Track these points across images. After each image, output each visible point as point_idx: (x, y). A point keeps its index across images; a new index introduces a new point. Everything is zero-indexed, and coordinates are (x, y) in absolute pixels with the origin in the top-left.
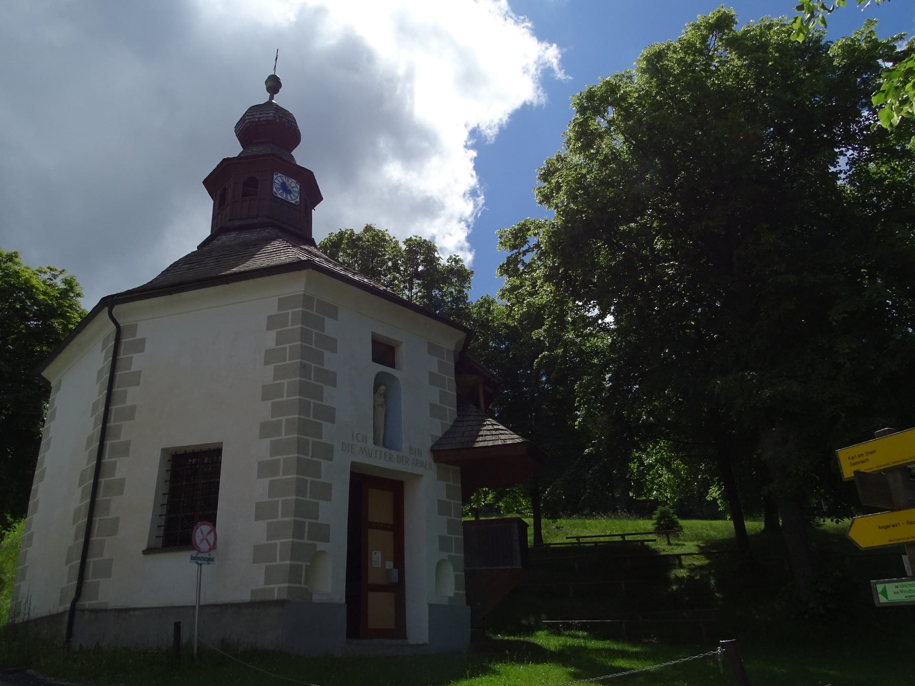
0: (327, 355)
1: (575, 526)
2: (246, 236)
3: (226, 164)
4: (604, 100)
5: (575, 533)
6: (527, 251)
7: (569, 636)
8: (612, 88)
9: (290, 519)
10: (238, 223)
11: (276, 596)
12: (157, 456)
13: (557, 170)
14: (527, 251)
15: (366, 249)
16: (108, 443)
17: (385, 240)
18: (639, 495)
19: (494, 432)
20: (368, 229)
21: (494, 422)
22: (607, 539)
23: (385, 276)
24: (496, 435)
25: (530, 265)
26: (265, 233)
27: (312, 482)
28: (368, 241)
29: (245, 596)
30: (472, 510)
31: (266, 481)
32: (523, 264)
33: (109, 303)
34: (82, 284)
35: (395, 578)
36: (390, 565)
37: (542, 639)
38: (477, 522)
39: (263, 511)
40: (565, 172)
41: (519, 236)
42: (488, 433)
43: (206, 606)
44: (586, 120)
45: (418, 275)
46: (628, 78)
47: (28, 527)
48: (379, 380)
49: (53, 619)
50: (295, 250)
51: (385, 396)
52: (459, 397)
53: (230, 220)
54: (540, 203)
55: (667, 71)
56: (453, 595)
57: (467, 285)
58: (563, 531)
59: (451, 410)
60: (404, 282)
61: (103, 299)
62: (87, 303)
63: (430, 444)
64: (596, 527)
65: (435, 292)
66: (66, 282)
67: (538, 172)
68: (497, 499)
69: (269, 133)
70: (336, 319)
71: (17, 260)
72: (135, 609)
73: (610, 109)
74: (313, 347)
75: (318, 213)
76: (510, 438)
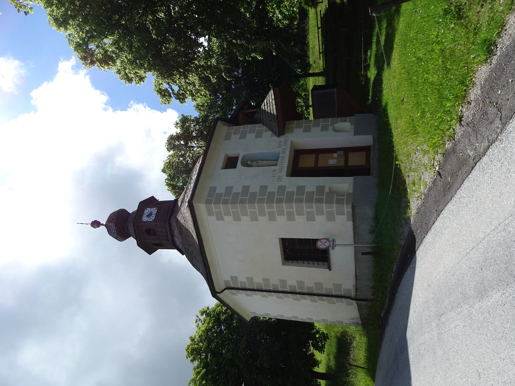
0: (234, 191)
1: (313, 53)
2: (176, 232)
4: (85, 51)
5: (317, 54)
6: (171, 89)
7: (370, 60)
8: (78, 47)
9: (314, 205)
10: (170, 237)
12: (285, 267)
13: (126, 74)
14: (171, 89)
15: (177, 172)
16: (280, 289)
17: (170, 162)
18: (296, 18)
19: (268, 105)
20: (164, 171)
21: (263, 104)
22: (320, 35)
23: (188, 160)
24: (269, 103)
25: (179, 87)
26: (174, 224)
27: (296, 195)
28: (171, 171)
29: (350, 224)
30: (306, 110)
31: (297, 217)
32: (179, 90)
33: (214, 294)
34: (203, 306)
35: (341, 153)
36: (335, 155)
37: (372, 73)
38: (313, 106)
39: (311, 218)
40: (127, 71)
41: (164, 94)
42: (269, 108)
43: (354, 241)
44: (98, 60)
45: (186, 144)
46: (70, 36)
47: (318, 321)
48: (245, 164)
49: (360, 308)
50: (182, 209)
51: (252, 161)
52: (251, 123)
54: (143, 81)
55: (65, 14)
56: (350, 124)
57: (189, 117)
58: (316, 58)
59: (258, 127)
60: (190, 150)
62: (212, 302)
63: (276, 137)
64: (314, 41)
65: (194, 134)
66: (202, 314)
67: (128, 84)
68: (300, 96)
69: (121, 225)
70: (216, 187)
71: (193, 337)
72: (356, 273)
73: (90, 47)
75: (161, 198)
76: (271, 96)
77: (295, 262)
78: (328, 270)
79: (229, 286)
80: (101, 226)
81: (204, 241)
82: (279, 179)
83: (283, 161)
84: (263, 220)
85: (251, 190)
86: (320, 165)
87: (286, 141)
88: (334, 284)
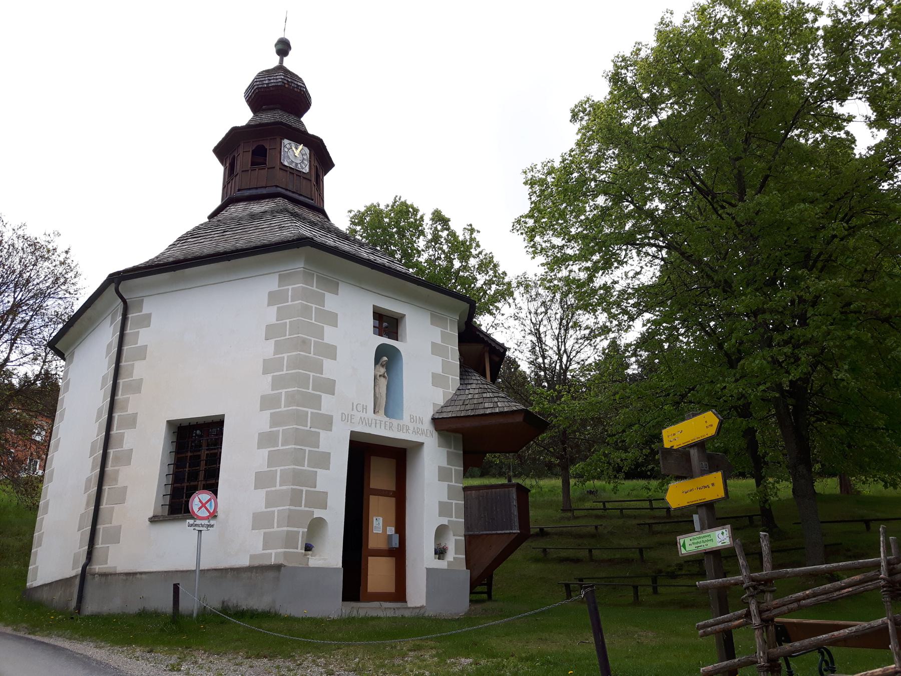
10: (247, 193)
11: (273, 561)
16: (116, 415)
29: (244, 561)
35: (395, 543)
36: (391, 530)
48: (381, 352)
49: (65, 583)
52: (462, 366)
59: (454, 378)
61: (111, 275)
69: (279, 98)
72: (141, 573)
74: (313, 321)
78: (151, 515)
79: (130, 310)
80: (278, 58)
81: (227, 262)
82: (346, 418)
83: (378, 426)
84: (265, 384)
85: (327, 363)
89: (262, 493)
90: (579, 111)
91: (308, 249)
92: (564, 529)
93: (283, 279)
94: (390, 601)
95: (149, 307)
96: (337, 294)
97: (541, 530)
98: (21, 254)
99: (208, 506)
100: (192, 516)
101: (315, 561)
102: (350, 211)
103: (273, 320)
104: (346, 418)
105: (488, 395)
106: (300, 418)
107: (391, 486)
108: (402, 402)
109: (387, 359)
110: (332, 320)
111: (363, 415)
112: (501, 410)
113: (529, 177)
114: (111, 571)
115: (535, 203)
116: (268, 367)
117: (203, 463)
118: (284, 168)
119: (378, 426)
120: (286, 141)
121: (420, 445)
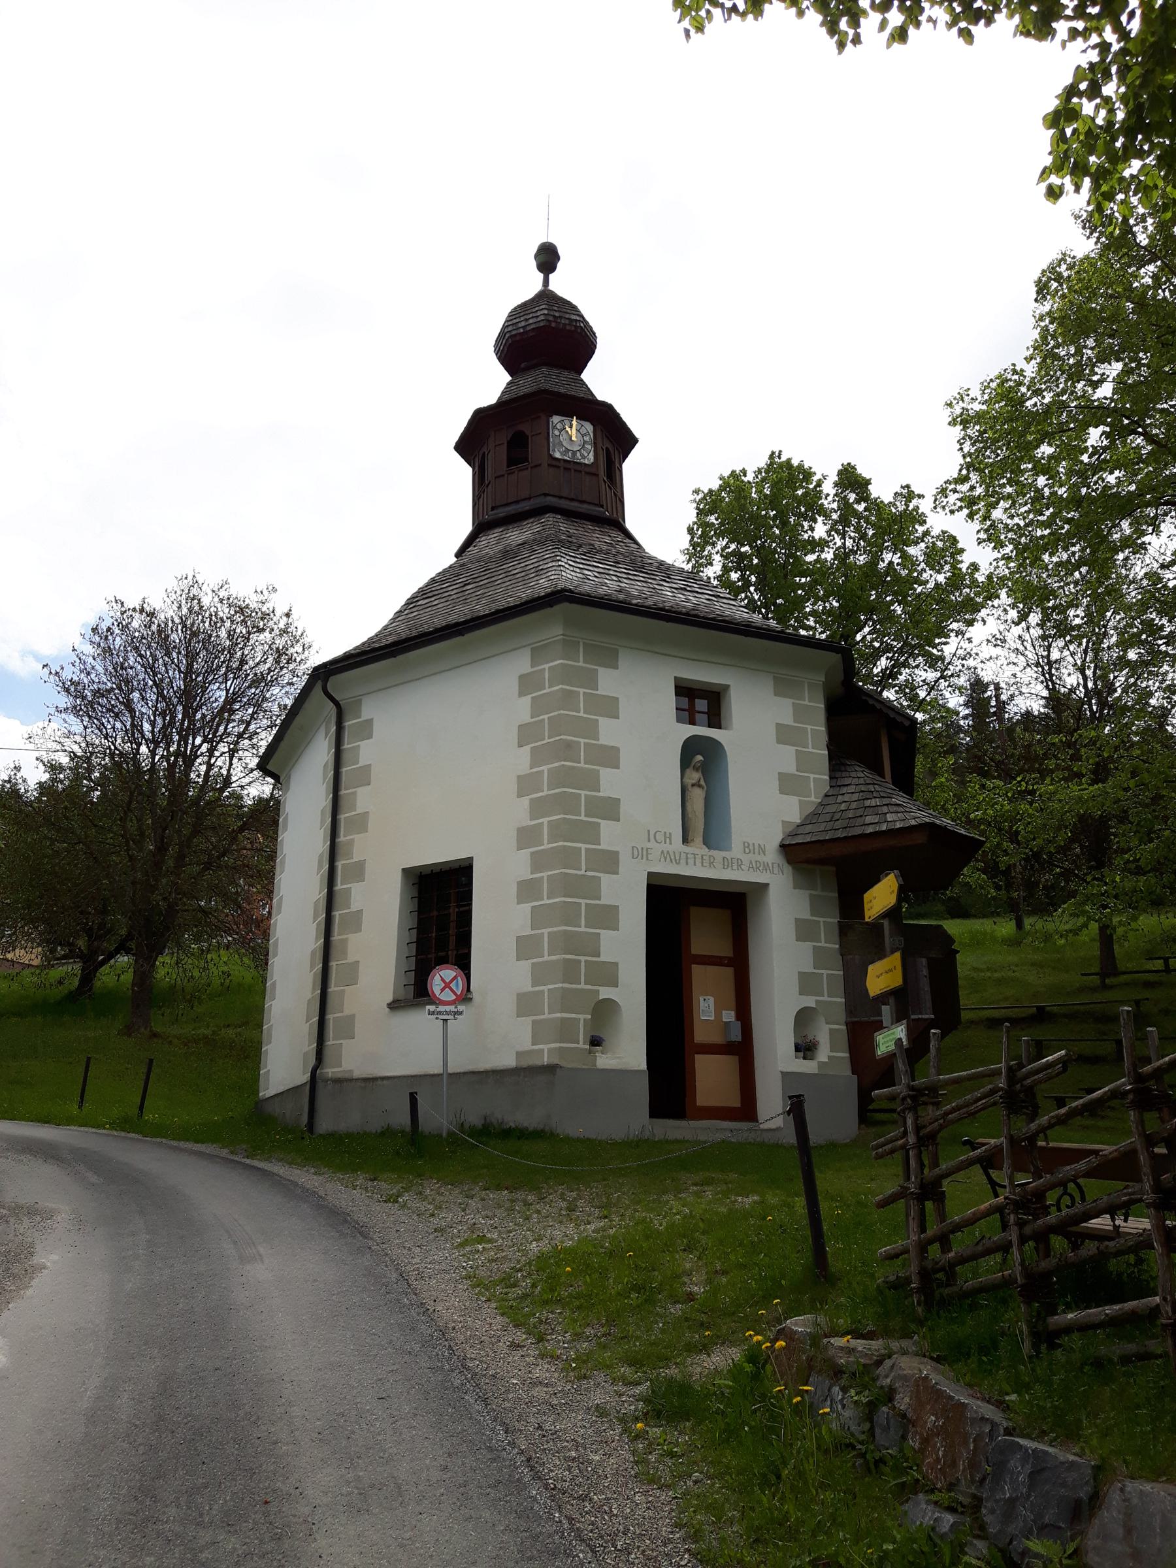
3: (482, 421)
10: (502, 512)
11: (546, 1061)
12: (397, 878)
16: (339, 864)
27: (585, 744)
29: (508, 1061)
31: (527, 907)
35: (736, 1035)
36: (729, 1016)
48: (690, 749)
52: (831, 757)
53: (493, 509)
59: (818, 778)
69: (547, 342)
77: (414, 905)
78: (390, 998)
80: (541, 275)
82: (640, 854)
83: (691, 861)
84: (519, 812)
85: (605, 774)
86: (697, 970)
87: (766, 867)
88: (354, 1016)
89: (526, 965)
90: (1050, 279)
91: (566, 605)
92: (1082, 1008)
93: (537, 655)
94: (723, 1119)
95: (370, 709)
96: (617, 668)
97: (1041, 1009)
98: (228, 624)
99: (453, 985)
100: (434, 1001)
101: (604, 1061)
102: (697, 492)
103: (526, 718)
104: (640, 854)
105: (873, 802)
106: (569, 857)
107: (723, 948)
108: (729, 821)
109: (701, 760)
110: (610, 707)
111: (666, 847)
112: (891, 826)
113: (958, 411)
114: (347, 1076)
115: (970, 455)
116: (525, 785)
117: (453, 925)
118: (555, 463)
119: (691, 861)
120: (556, 419)
121: (762, 888)
